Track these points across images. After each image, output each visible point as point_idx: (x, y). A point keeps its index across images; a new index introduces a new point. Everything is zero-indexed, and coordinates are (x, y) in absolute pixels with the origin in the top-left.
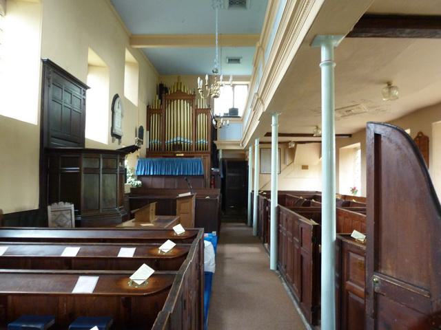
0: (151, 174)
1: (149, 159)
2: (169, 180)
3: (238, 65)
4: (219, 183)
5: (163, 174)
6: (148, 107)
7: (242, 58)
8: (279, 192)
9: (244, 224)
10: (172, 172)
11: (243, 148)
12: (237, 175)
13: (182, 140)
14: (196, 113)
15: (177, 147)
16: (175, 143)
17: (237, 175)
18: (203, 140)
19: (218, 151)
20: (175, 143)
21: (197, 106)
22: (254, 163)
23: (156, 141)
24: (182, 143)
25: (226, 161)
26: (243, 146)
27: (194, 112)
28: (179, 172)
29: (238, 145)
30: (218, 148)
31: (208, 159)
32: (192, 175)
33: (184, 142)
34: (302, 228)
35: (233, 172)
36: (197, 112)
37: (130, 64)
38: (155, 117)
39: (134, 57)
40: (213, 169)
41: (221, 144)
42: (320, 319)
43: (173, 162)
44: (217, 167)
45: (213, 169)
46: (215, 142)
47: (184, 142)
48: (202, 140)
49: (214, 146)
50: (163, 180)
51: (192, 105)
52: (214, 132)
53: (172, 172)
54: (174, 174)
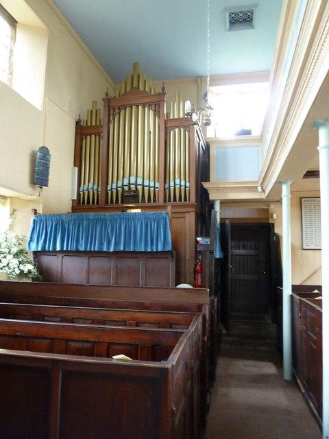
0: (58, 248)
1: (76, 215)
2: (96, 263)
3: (251, 31)
4: (210, 269)
5: (82, 249)
6: (78, 123)
7: (256, 6)
8: (293, 286)
9: (269, 369)
10: (101, 244)
11: (263, 196)
12: (251, 252)
13: (140, 181)
14: (166, 129)
15: (130, 197)
16: (126, 188)
17: (251, 252)
18: (182, 181)
19: (212, 205)
20: (126, 188)
21: (168, 114)
22: (286, 230)
23: (91, 186)
24: (140, 188)
25: (227, 222)
26: (263, 191)
27: (163, 126)
28: (117, 244)
29: (254, 189)
30: (212, 197)
31: (190, 219)
32: (145, 253)
33: (143, 186)
34: (184, 218)
35: (244, 247)
36: (168, 126)
37: (29, 28)
38: (90, 142)
39: (39, 15)
40: (198, 239)
41: (218, 189)
42: (281, 285)
43: (104, 221)
44: (207, 235)
45: (198, 239)
46: (206, 185)
47: (143, 186)
48: (177, 182)
49: (203, 194)
50: (110, 264)
51: (157, 113)
52: (203, 169)
53: (101, 244)
54: (105, 249)
